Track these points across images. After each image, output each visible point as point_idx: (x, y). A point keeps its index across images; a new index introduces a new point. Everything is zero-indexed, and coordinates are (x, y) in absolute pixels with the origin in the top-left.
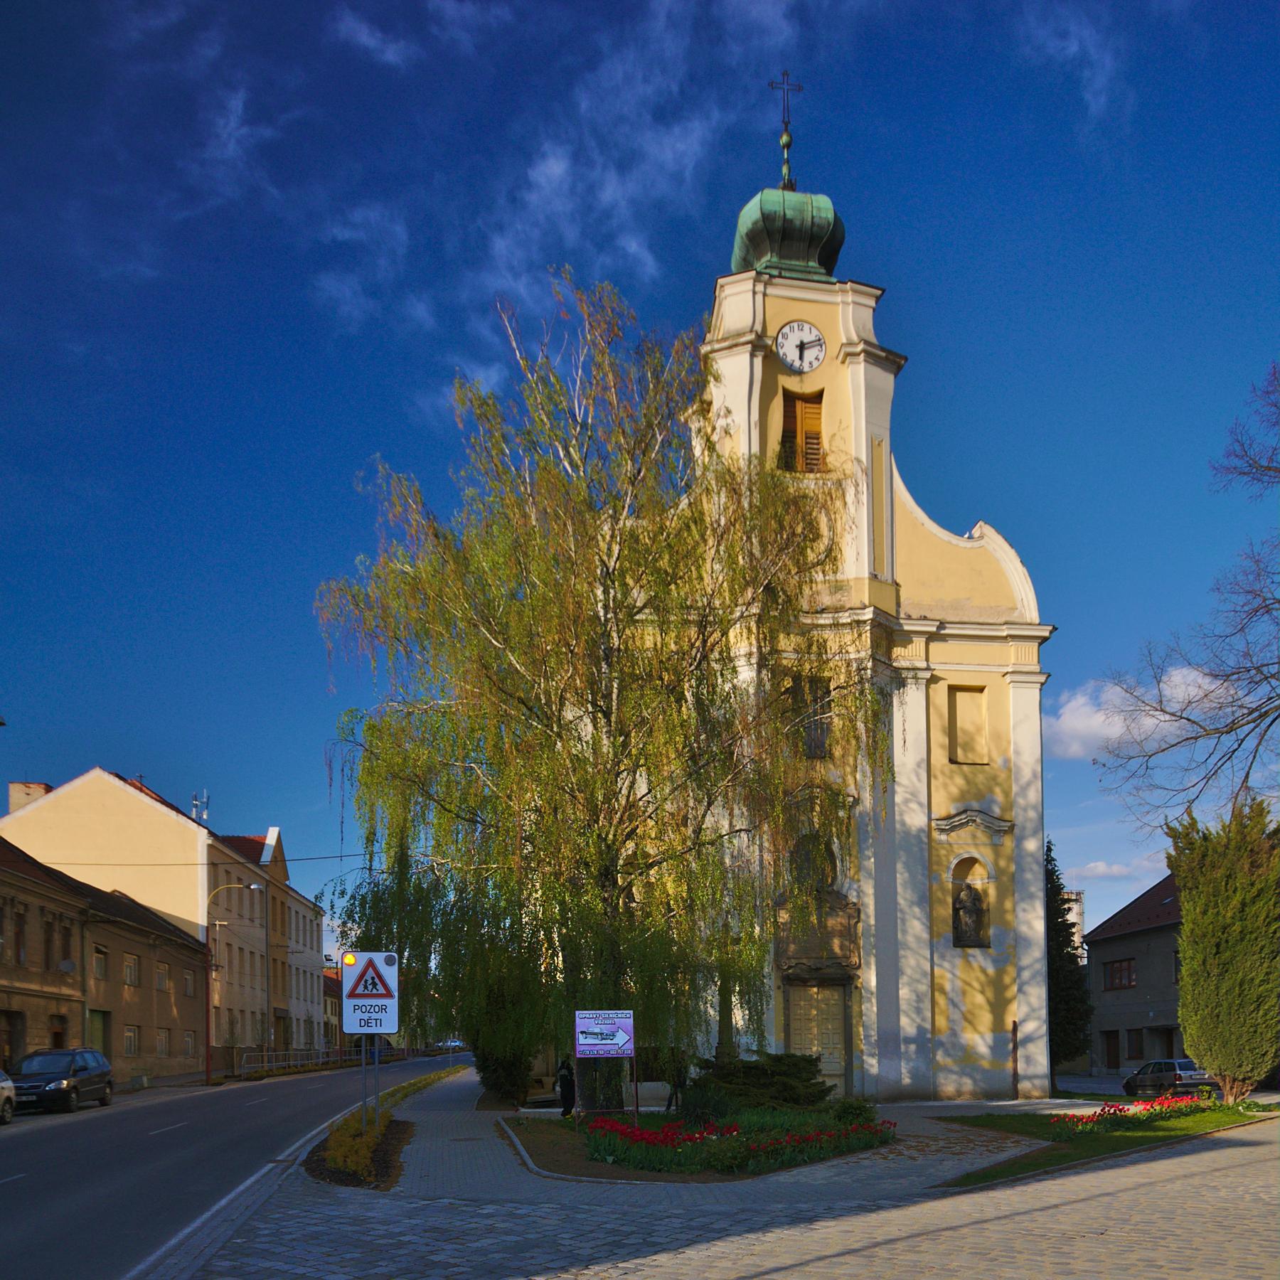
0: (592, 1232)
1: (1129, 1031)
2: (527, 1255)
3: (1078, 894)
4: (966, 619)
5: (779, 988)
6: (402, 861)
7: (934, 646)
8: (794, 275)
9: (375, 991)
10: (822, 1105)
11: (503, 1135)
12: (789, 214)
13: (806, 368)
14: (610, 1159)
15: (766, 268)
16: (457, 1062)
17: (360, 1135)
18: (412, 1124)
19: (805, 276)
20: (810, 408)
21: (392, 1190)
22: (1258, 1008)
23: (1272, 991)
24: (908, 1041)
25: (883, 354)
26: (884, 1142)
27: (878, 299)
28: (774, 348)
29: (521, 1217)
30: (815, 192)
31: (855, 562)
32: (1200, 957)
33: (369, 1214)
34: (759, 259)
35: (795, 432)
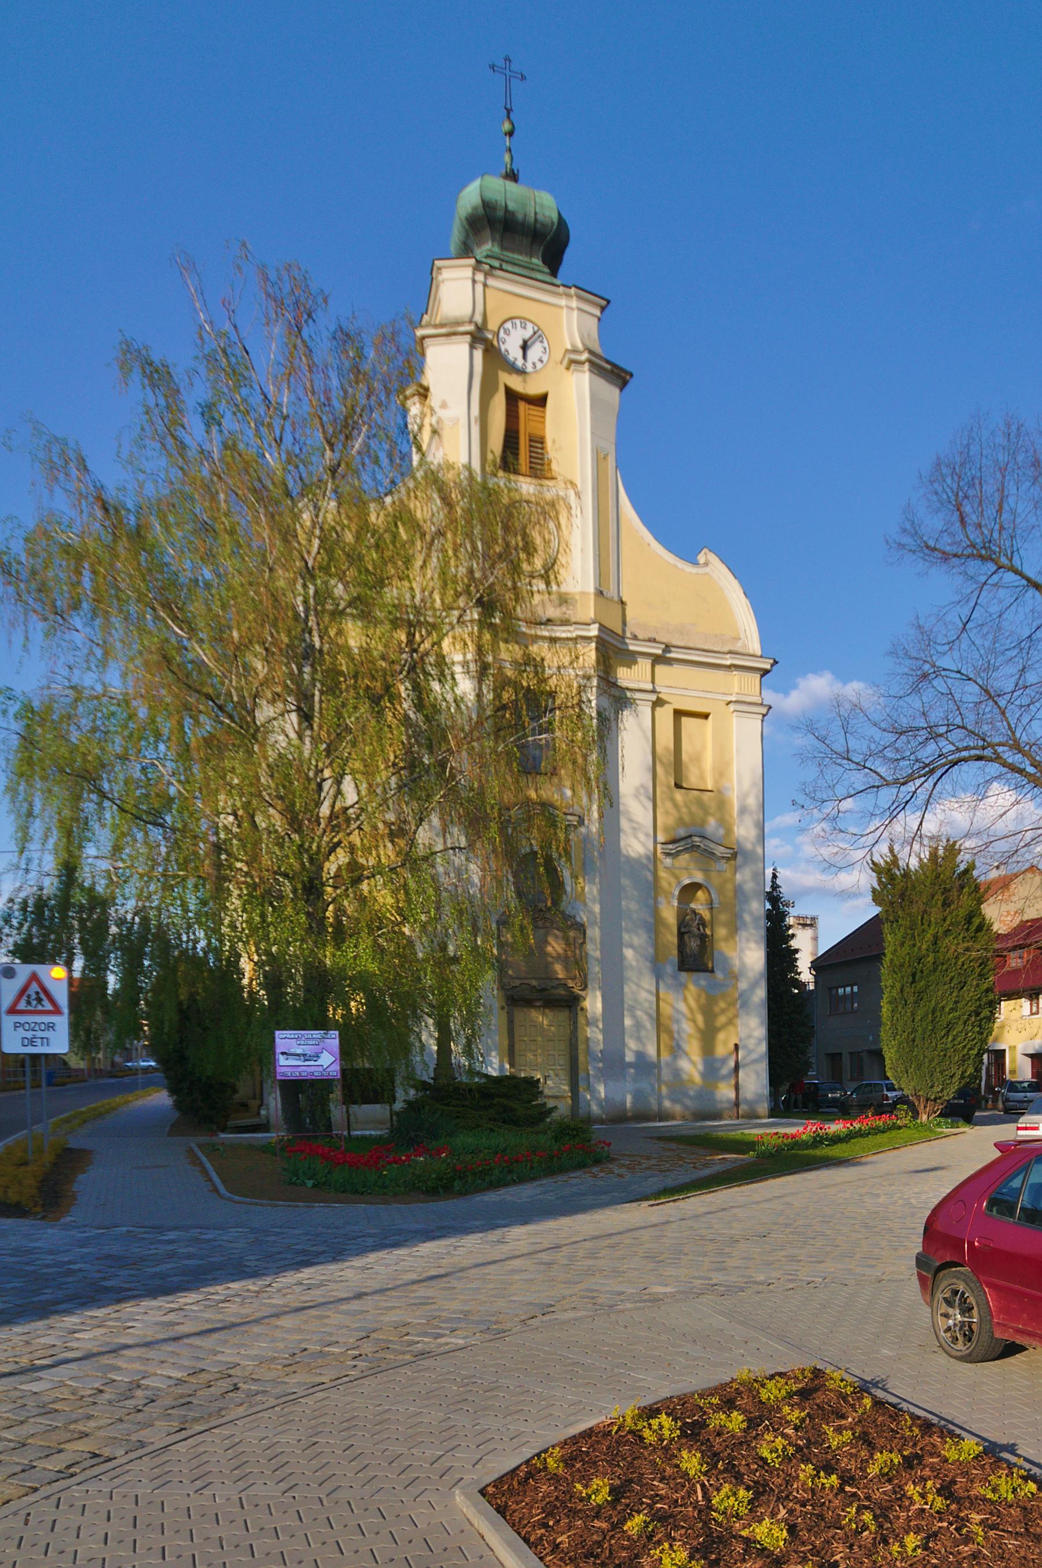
0: (280, 1253)
1: (851, 1053)
2: (209, 1277)
3: (813, 919)
4: (692, 645)
5: (502, 1008)
6: (69, 871)
7: (660, 669)
8: (517, 270)
9: (40, 1008)
10: (541, 1127)
11: (195, 1161)
12: (511, 206)
13: (529, 368)
14: (310, 1183)
15: (487, 257)
16: (146, 1085)
17: (25, 1164)
18: (90, 1152)
19: (527, 274)
20: (534, 410)
21: (62, 1220)
22: (947, 1034)
23: (959, 1018)
24: (630, 1065)
25: (609, 367)
26: (597, 1162)
27: (603, 309)
28: (495, 343)
29: (208, 1241)
30: (540, 188)
31: (578, 574)
32: (898, 985)
33: (37, 1245)
34: (479, 245)
35: (517, 432)
